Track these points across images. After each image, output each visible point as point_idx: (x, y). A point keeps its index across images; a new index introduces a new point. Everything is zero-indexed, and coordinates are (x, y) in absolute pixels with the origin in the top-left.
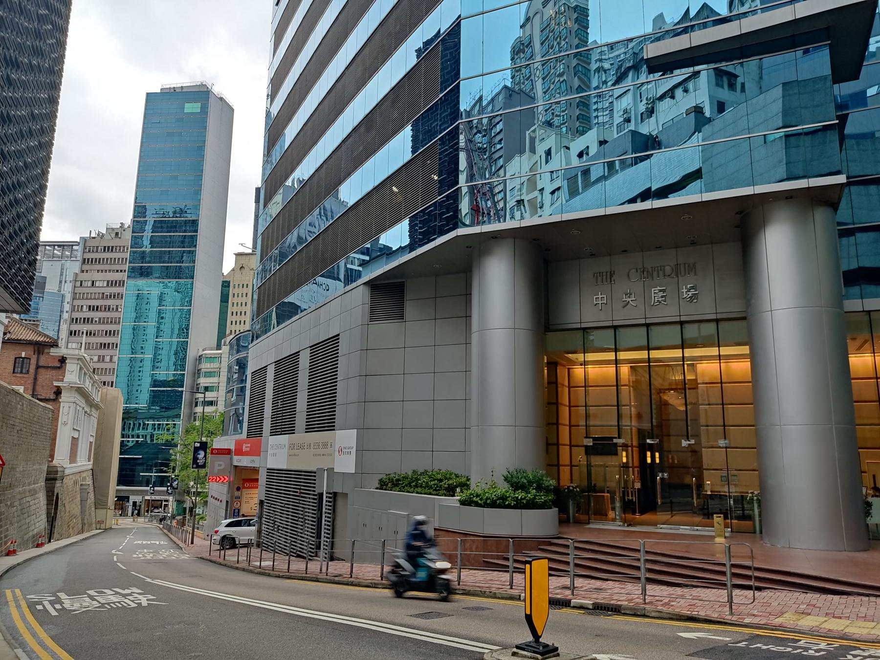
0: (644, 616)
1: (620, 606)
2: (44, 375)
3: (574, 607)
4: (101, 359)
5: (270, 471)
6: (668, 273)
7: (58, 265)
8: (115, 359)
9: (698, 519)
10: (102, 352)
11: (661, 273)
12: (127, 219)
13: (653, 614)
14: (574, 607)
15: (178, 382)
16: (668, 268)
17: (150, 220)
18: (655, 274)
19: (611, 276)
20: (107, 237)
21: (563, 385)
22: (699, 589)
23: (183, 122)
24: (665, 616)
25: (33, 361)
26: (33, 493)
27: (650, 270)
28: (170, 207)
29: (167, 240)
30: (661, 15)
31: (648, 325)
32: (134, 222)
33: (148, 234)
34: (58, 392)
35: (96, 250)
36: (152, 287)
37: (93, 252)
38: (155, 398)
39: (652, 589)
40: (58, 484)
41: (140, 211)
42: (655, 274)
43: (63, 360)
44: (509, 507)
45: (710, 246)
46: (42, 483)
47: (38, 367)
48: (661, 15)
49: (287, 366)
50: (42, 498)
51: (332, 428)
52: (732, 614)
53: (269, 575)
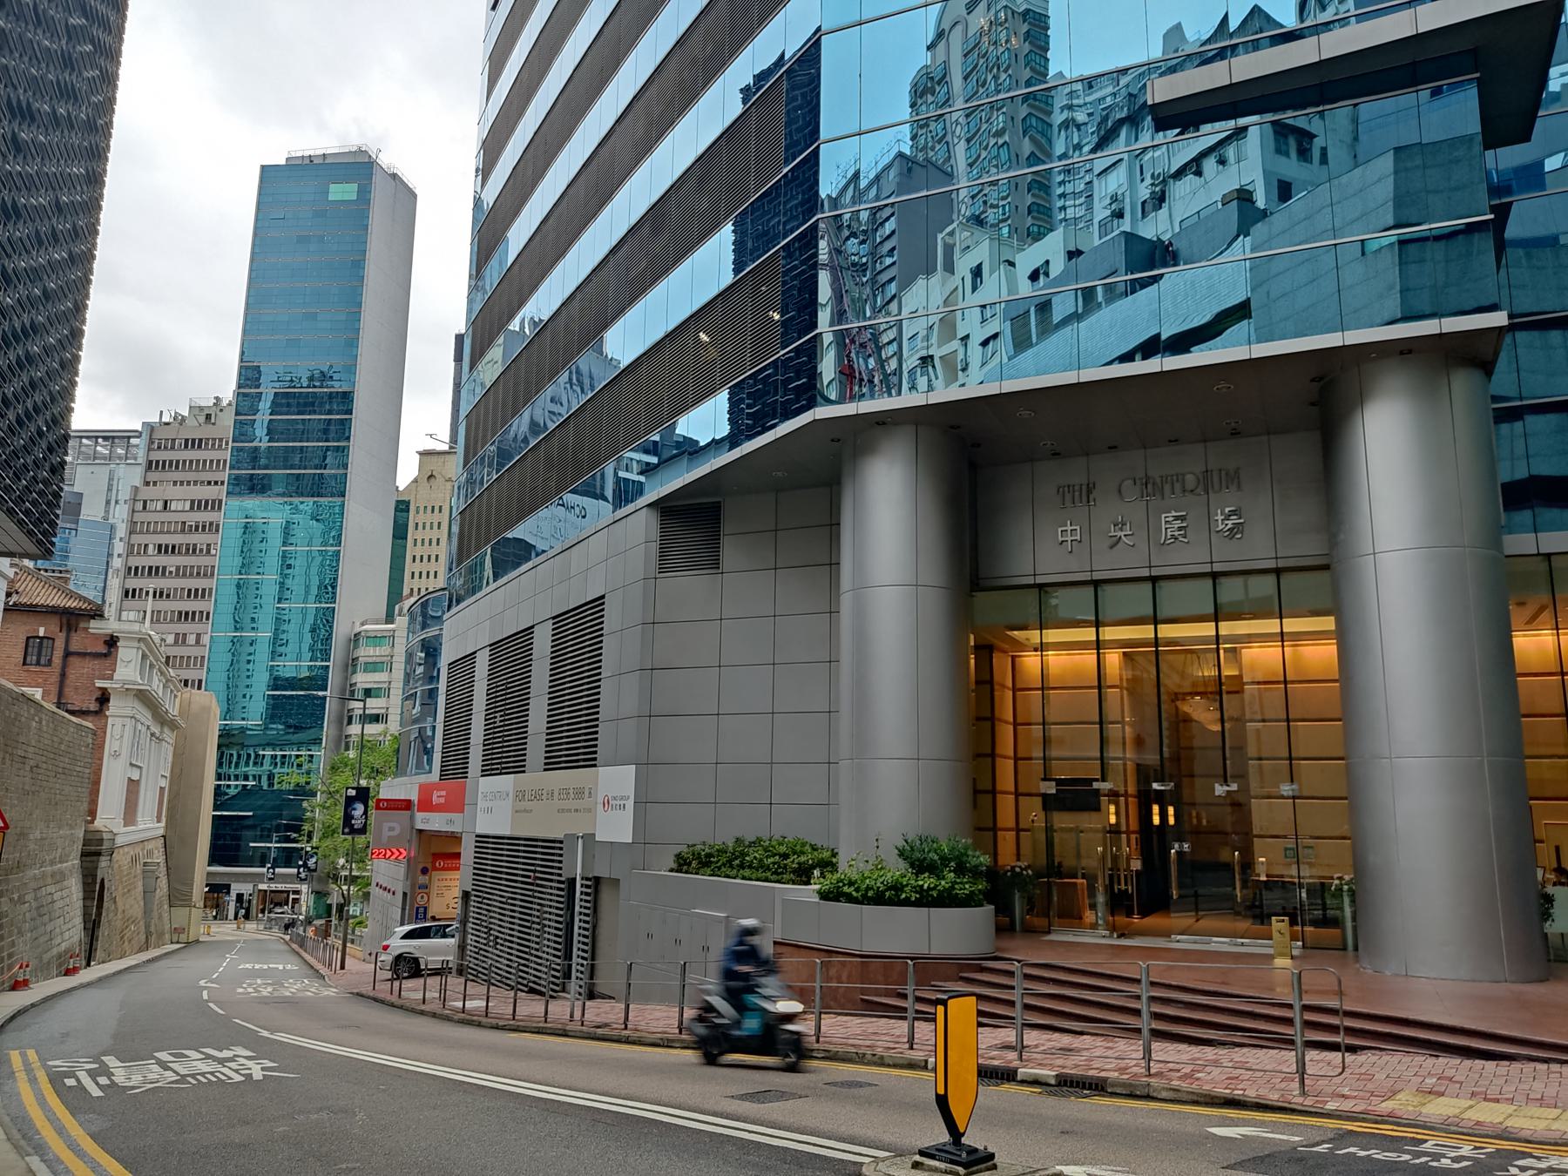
0: (1148, 1097)
1: (1105, 1080)
2: (78, 669)
3: (1023, 1082)
4: (181, 639)
5: (482, 839)
6: (1190, 486)
7: (103, 473)
8: (206, 639)
9: (1244, 925)
10: (182, 628)
11: (1178, 486)
12: (227, 389)
13: (1164, 1095)
14: (1023, 1082)
15: (318, 681)
16: (1190, 478)
17: (268, 392)
18: (1167, 488)
19: (1089, 492)
20: (191, 422)
21: (1003, 686)
22: (1245, 1050)
24: (1185, 1097)
25: (60, 644)
26: (59, 878)
27: (1158, 480)
28: (302, 368)
29: (297, 427)
30: (1178, 27)
31: (1154, 580)
32: (239, 395)
33: (263, 416)
34: (104, 698)
35: (171, 445)
36: (271, 512)
37: (165, 449)
38: (277, 709)
39: (1162, 1050)
40: (103, 862)
41: (249, 376)
42: (1167, 488)
43: (112, 642)
44: (907, 903)
45: (1265, 438)
46: (75, 861)
47: (67, 654)
48: (1178, 27)
49: (511, 652)
50: (74, 887)
52: (1304, 1093)
53: (479, 1025)
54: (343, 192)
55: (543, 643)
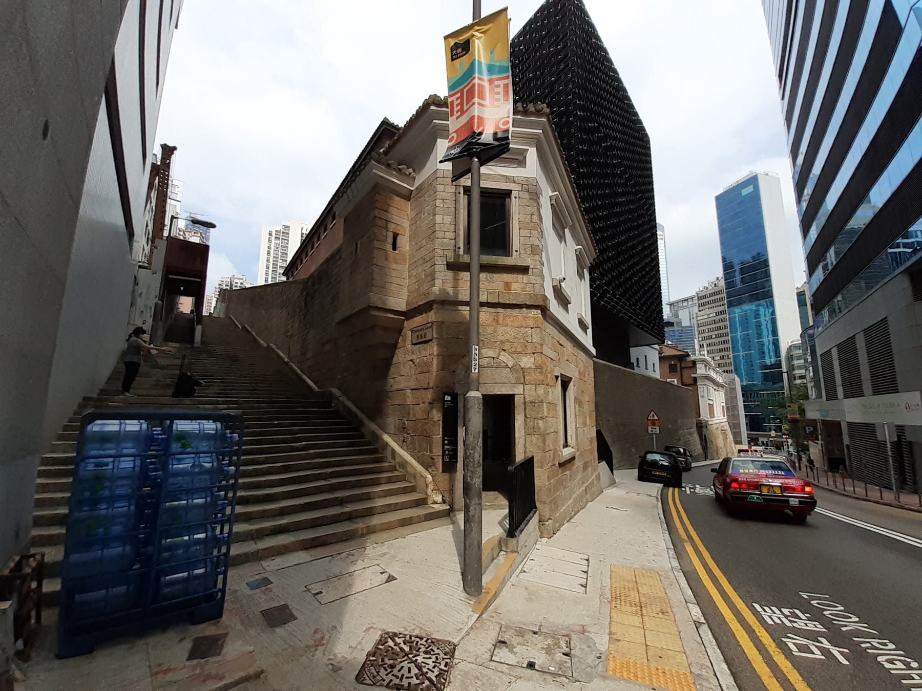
2: (685, 372)
4: (722, 358)
5: (850, 424)
7: (687, 311)
8: (731, 356)
10: (721, 354)
12: (720, 273)
15: (778, 365)
17: (737, 268)
20: (710, 288)
23: (739, 210)
25: (678, 365)
26: (690, 434)
28: (748, 257)
29: (747, 278)
30: (191, 657)
32: (725, 274)
33: (738, 278)
34: (695, 379)
35: (705, 297)
36: (749, 307)
37: (704, 300)
38: (766, 377)
40: (704, 429)
41: (728, 267)
43: (694, 362)
46: (694, 429)
47: (682, 368)
48: (191, 657)
49: (847, 348)
50: (696, 437)
51: (896, 391)
53: (850, 497)
54: (750, 189)
55: (835, 352)
